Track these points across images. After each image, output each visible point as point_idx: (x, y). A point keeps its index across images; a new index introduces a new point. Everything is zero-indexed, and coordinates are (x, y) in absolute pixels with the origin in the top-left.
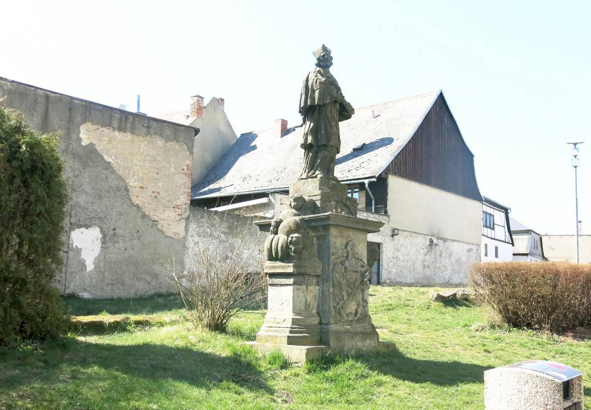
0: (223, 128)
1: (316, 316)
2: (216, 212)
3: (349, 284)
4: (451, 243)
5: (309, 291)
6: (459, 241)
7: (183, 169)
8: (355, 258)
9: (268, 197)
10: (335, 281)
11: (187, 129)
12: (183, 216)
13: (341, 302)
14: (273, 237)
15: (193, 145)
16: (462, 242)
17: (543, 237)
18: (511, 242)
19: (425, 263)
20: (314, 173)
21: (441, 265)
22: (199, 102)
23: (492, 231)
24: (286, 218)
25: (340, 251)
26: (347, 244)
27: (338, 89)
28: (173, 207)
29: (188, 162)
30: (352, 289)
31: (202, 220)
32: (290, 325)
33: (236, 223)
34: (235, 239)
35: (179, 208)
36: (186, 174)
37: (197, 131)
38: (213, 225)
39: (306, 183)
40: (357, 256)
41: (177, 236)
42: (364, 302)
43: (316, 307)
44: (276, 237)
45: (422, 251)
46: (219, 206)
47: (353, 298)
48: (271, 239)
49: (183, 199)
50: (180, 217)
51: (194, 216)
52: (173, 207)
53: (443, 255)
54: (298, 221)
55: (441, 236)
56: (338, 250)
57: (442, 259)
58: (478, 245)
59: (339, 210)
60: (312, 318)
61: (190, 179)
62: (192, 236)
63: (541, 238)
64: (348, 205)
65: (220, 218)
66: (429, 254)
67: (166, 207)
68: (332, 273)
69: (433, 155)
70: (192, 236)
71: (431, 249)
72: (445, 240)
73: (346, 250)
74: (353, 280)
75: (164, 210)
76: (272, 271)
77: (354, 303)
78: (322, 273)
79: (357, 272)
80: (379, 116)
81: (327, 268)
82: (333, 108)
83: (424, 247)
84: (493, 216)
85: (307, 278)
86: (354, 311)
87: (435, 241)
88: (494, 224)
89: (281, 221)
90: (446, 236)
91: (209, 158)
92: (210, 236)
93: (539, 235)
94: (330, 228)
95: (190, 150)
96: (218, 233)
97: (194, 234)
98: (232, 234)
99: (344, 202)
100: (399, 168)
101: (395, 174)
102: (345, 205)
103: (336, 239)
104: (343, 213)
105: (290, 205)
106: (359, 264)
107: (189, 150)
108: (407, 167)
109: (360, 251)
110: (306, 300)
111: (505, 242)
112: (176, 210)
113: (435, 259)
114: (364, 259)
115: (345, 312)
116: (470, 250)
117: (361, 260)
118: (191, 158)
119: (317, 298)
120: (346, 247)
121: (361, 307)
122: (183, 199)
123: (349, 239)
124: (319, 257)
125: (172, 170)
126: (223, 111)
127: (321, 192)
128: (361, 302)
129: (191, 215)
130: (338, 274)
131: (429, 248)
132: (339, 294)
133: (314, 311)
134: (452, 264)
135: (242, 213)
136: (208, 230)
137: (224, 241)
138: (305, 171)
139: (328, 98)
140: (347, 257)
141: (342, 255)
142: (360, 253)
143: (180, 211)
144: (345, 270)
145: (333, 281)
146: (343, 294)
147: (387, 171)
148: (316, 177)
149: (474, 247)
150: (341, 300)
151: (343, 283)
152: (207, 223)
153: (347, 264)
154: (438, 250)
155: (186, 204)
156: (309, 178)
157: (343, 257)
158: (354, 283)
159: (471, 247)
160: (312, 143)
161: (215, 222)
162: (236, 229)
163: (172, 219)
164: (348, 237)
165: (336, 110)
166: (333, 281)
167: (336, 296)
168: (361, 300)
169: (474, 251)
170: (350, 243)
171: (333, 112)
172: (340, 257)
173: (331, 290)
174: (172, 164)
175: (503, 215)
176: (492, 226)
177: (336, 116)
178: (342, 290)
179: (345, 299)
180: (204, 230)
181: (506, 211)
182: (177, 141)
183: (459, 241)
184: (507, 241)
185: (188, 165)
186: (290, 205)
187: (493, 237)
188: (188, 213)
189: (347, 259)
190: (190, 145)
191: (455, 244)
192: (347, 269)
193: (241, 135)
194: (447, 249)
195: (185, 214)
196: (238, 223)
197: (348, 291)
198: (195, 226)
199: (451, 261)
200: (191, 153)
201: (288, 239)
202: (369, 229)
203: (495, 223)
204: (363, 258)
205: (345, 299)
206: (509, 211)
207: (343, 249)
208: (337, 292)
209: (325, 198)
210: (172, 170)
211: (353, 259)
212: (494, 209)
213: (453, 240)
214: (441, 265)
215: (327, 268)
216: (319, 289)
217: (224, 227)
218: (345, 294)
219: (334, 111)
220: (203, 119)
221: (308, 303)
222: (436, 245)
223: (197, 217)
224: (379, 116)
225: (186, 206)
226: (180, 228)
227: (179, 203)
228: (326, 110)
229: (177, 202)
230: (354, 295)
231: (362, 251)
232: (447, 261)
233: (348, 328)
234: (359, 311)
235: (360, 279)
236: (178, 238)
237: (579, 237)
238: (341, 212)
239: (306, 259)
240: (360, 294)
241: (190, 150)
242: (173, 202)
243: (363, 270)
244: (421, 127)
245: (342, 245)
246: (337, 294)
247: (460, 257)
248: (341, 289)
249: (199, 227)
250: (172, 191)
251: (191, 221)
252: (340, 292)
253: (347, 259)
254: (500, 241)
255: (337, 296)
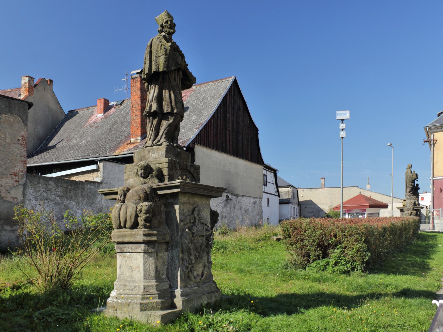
0: (52, 105)
1: (166, 281)
2: (51, 178)
3: (196, 248)
4: (242, 198)
5: (159, 257)
6: (247, 196)
7: (19, 140)
8: (201, 223)
9: (97, 164)
10: (184, 246)
11: (20, 102)
12: (20, 182)
13: (190, 266)
14: (120, 206)
15: (27, 117)
16: (249, 196)
17: (299, 190)
18: (278, 195)
19: (223, 214)
20: (159, 141)
21: (234, 215)
22: (30, 82)
23: (265, 187)
24: (133, 187)
25: (188, 217)
26: (194, 210)
27: (183, 56)
28: (11, 175)
29: (23, 133)
30: (199, 252)
31: (38, 186)
32: (141, 291)
33: (69, 187)
34: (69, 201)
35: (16, 175)
36: (21, 144)
37: (30, 105)
38: (49, 190)
39: (151, 151)
40: (202, 221)
41: (15, 200)
42: (209, 263)
43: (165, 272)
44: (124, 205)
45: (220, 205)
46: (52, 172)
47: (200, 260)
48: (119, 208)
49: (19, 167)
50: (18, 183)
51: (31, 182)
52: (11, 175)
53: (236, 208)
54: (429, 261)
55: (235, 193)
56: (186, 216)
57: (235, 210)
58: (261, 199)
59: (184, 178)
60: (163, 283)
61: (26, 149)
62: (30, 200)
63: (298, 191)
64: (192, 172)
65: (55, 183)
66: (226, 207)
67: (3, 174)
68: (181, 239)
69: (229, 128)
70: (30, 200)
71: (227, 203)
72: (237, 196)
73: (192, 216)
74: (200, 244)
75: (2, 178)
76: (120, 240)
77: (201, 265)
78: (170, 240)
79: (203, 236)
80: (62, 140)
81: (176, 234)
82: (176, 75)
83: (222, 202)
84: (266, 176)
85: (157, 246)
86: (201, 272)
87: (230, 196)
88: (267, 182)
89: (128, 190)
90: (238, 193)
91: (40, 130)
92: (47, 199)
93: (296, 189)
94: (178, 196)
95: (25, 122)
96: (53, 196)
97: (32, 198)
98: (67, 197)
99: (189, 169)
100: (204, 139)
101: (200, 144)
102: (190, 172)
103: (184, 206)
104: (188, 180)
105: (137, 173)
106: (205, 228)
107: (23, 122)
108: (210, 139)
109: (205, 215)
110: (157, 267)
111: (274, 195)
112: (14, 177)
113: (231, 210)
114: (208, 223)
115: (193, 275)
116: (255, 203)
117: (206, 225)
118: (25, 130)
119: (166, 263)
120: (193, 213)
121: (207, 268)
122: (19, 167)
123: (195, 206)
124: (167, 225)
125: (8, 140)
126: (52, 90)
127: (169, 160)
128: (207, 264)
129: (28, 181)
130: (187, 239)
131: (226, 202)
132: (188, 258)
133: (164, 277)
134: (242, 214)
135: (74, 178)
136: (45, 194)
137: (59, 204)
138: (150, 139)
139: (173, 65)
140: (194, 223)
141: (190, 221)
142: (205, 218)
143: (17, 177)
144: (192, 236)
145: (182, 246)
146: (192, 258)
147: (194, 142)
148: (161, 144)
149: (258, 200)
150: (190, 264)
151: (191, 248)
152: (43, 188)
153: (195, 229)
154: (232, 204)
155: (22, 172)
156: (154, 145)
157: (190, 223)
158: (201, 247)
159: (256, 200)
160: (157, 111)
161: (50, 187)
162: (70, 193)
163: (10, 185)
164: (194, 203)
165: (179, 78)
166: (182, 246)
167: (185, 261)
168: (206, 261)
169: (257, 203)
170: (197, 209)
171: (176, 80)
172: (188, 223)
173: (181, 255)
174: (7, 135)
175: (273, 175)
176: (265, 184)
177: (180, 85)
178: (191, 254)
179: (193, 263)
180: (40, 194)
181: (275, 172)
182: (11, 114)
183: (247, 196)
184: (275, 194)
185: (23, 136)
186: (137, 173)
187: (266, 191)
188: (25, 179)
189: (195, 225)
190: (24, 118)
191: (245, 198)
192: (195, 234)
193: (69, 111)
194: (239, 202)
195: (22, 180)
196: (71, 187)
197: (195, 255)
198: (32, 191)
199: (242, 211)
200: (26, 125)
201: (137, 208)
202: (213, 195)
203: (267, 181)
204: (208, 222)
205: (193, 263)
206: (277, 172)
207: (190, 215)
208: (186, 256)
209: (171, 166)
210: (8, 140)
211: (200, 224)
212: (270, 172)
213: (243, 196)
214: (234, 215)
215: (176, 234)
216: (168, 255)
217: (59, 191)
218: (193, 258)
219: (176, 79)
220: (34, 97)
221: (158, 269)
222: (231, 200)
223: (34, 183)
224: (62, 140)
225: (22, 174)
226: (17, 193)
227: (16, 170)
228: (170, 77)
229: (14, 170)
230: (201, 258)
231: (206, 216)
232: (238, 212)
233: (196, 289)
234: (206, 273)
235: (205, 242)
236: (17, 202)
237: (394, 198)
238: (186, 179)
239: (155, 227)
240: (205, 256)
241: (25, 122)
242: (10, 170)
243: (208, 233)
244: (220, 107)
245: (189, 211)
246: (186, 259)
247: (248, 208)
248: (190, 254)
249: (35, 191)
250: (9, 159)
251: (28, 187)
252: (189, 257)
253: (195, 225)
254: (270, 194)
255: (187, 261)
